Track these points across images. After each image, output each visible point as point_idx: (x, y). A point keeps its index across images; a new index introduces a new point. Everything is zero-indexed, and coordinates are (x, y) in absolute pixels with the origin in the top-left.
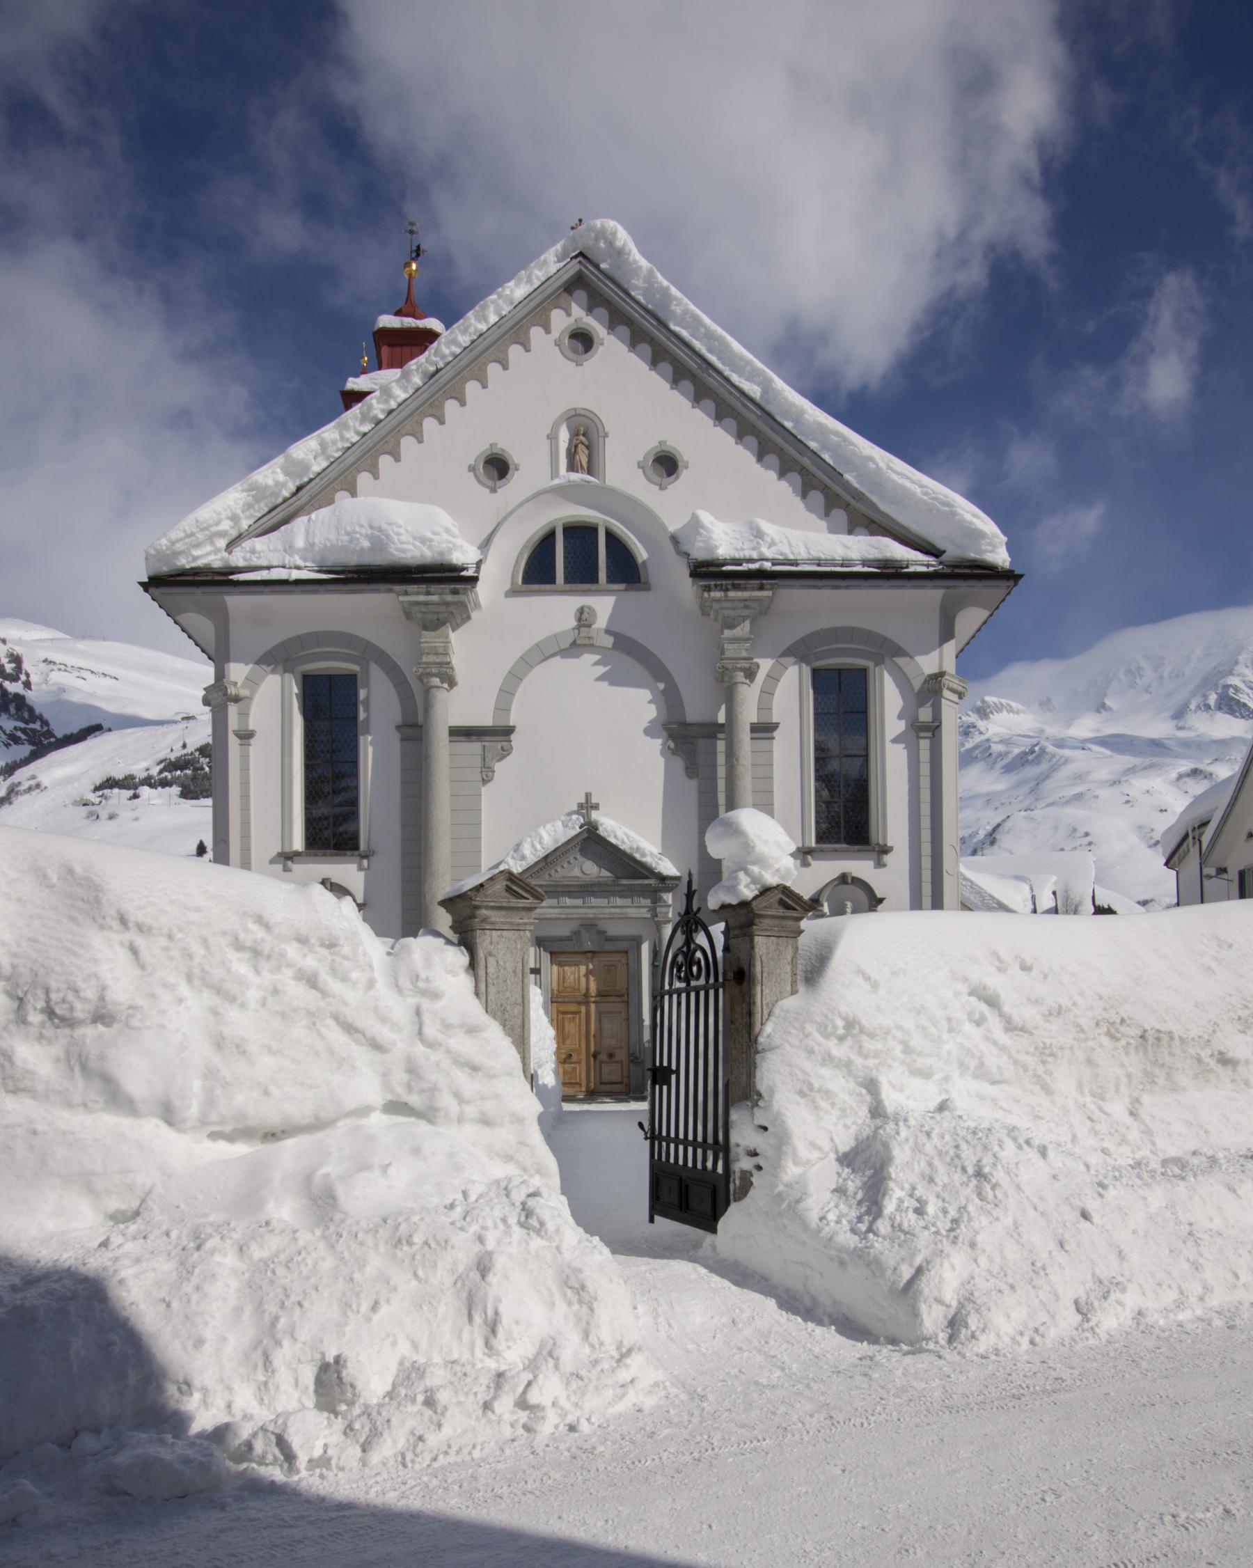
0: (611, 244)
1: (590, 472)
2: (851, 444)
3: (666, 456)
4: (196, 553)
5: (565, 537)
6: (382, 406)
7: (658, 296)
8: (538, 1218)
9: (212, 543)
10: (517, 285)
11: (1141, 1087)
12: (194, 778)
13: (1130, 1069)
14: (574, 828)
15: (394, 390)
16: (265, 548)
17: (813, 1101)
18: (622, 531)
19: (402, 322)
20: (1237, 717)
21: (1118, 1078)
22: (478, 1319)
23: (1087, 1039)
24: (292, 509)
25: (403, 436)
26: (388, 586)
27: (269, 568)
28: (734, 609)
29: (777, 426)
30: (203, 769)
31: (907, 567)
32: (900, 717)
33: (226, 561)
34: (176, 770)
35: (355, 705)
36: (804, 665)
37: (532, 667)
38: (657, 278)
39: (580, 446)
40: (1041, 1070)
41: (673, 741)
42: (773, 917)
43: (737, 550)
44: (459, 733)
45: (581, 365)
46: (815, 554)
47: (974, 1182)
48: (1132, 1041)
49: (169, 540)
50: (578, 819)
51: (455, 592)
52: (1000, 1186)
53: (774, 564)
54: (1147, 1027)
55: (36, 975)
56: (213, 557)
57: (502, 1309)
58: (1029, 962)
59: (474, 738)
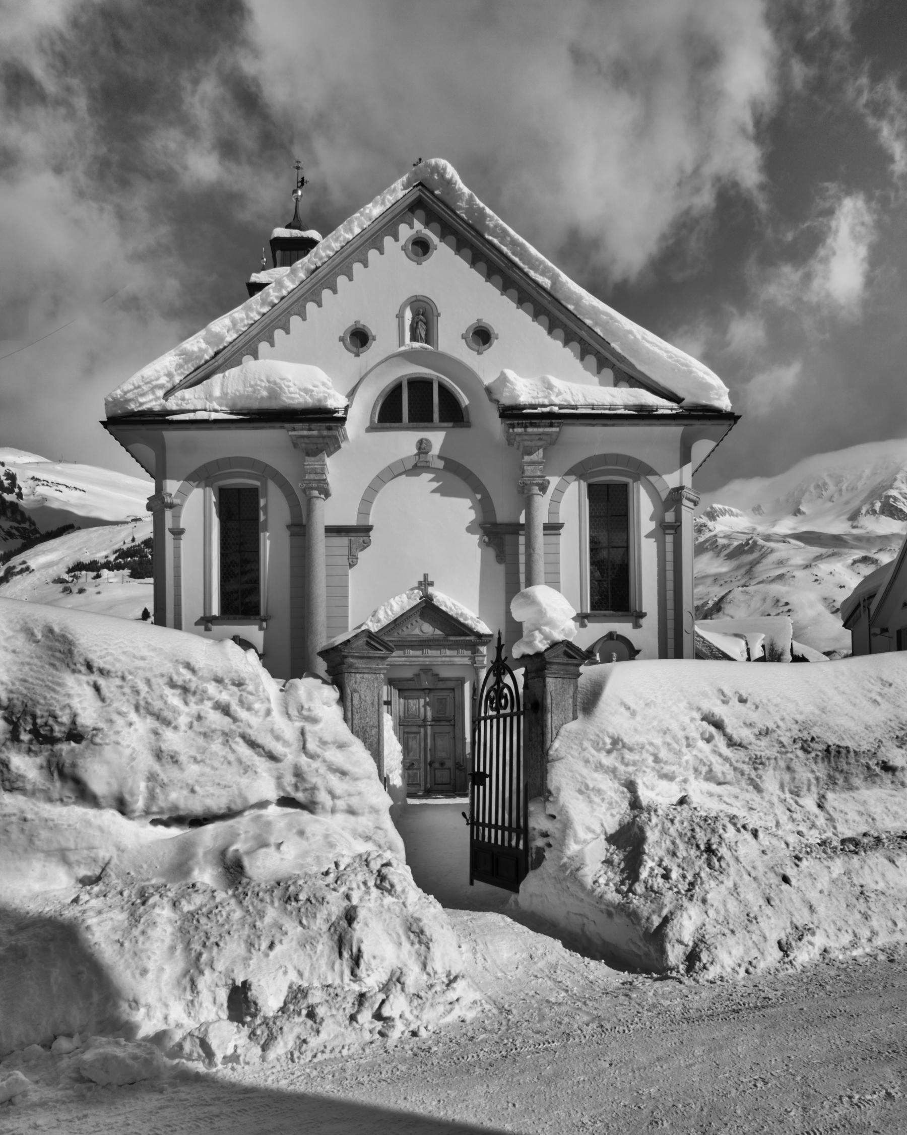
1: (427, 342)
2: (616, 321)
4: (142, 400)
6: (276, 294)
9: (154, 393)
10: (374, 206)
13: (818, 774)
16: (192, 396)
17: (589, 797)
21: (809, 780)
22: (346, 955)
23: (787, 752)
24: (211, 368)
27: (194, 411)
32: (651, 519)
36: (582, 482)
40: (753, 774)
43: (533, 398)
44: (333, 531)
46: (591, 401)
48: (820, 754)
49: (122, 391)
51: (329, 429)
53: (560, 408)
54: (830, 743)
59: (343, 534)
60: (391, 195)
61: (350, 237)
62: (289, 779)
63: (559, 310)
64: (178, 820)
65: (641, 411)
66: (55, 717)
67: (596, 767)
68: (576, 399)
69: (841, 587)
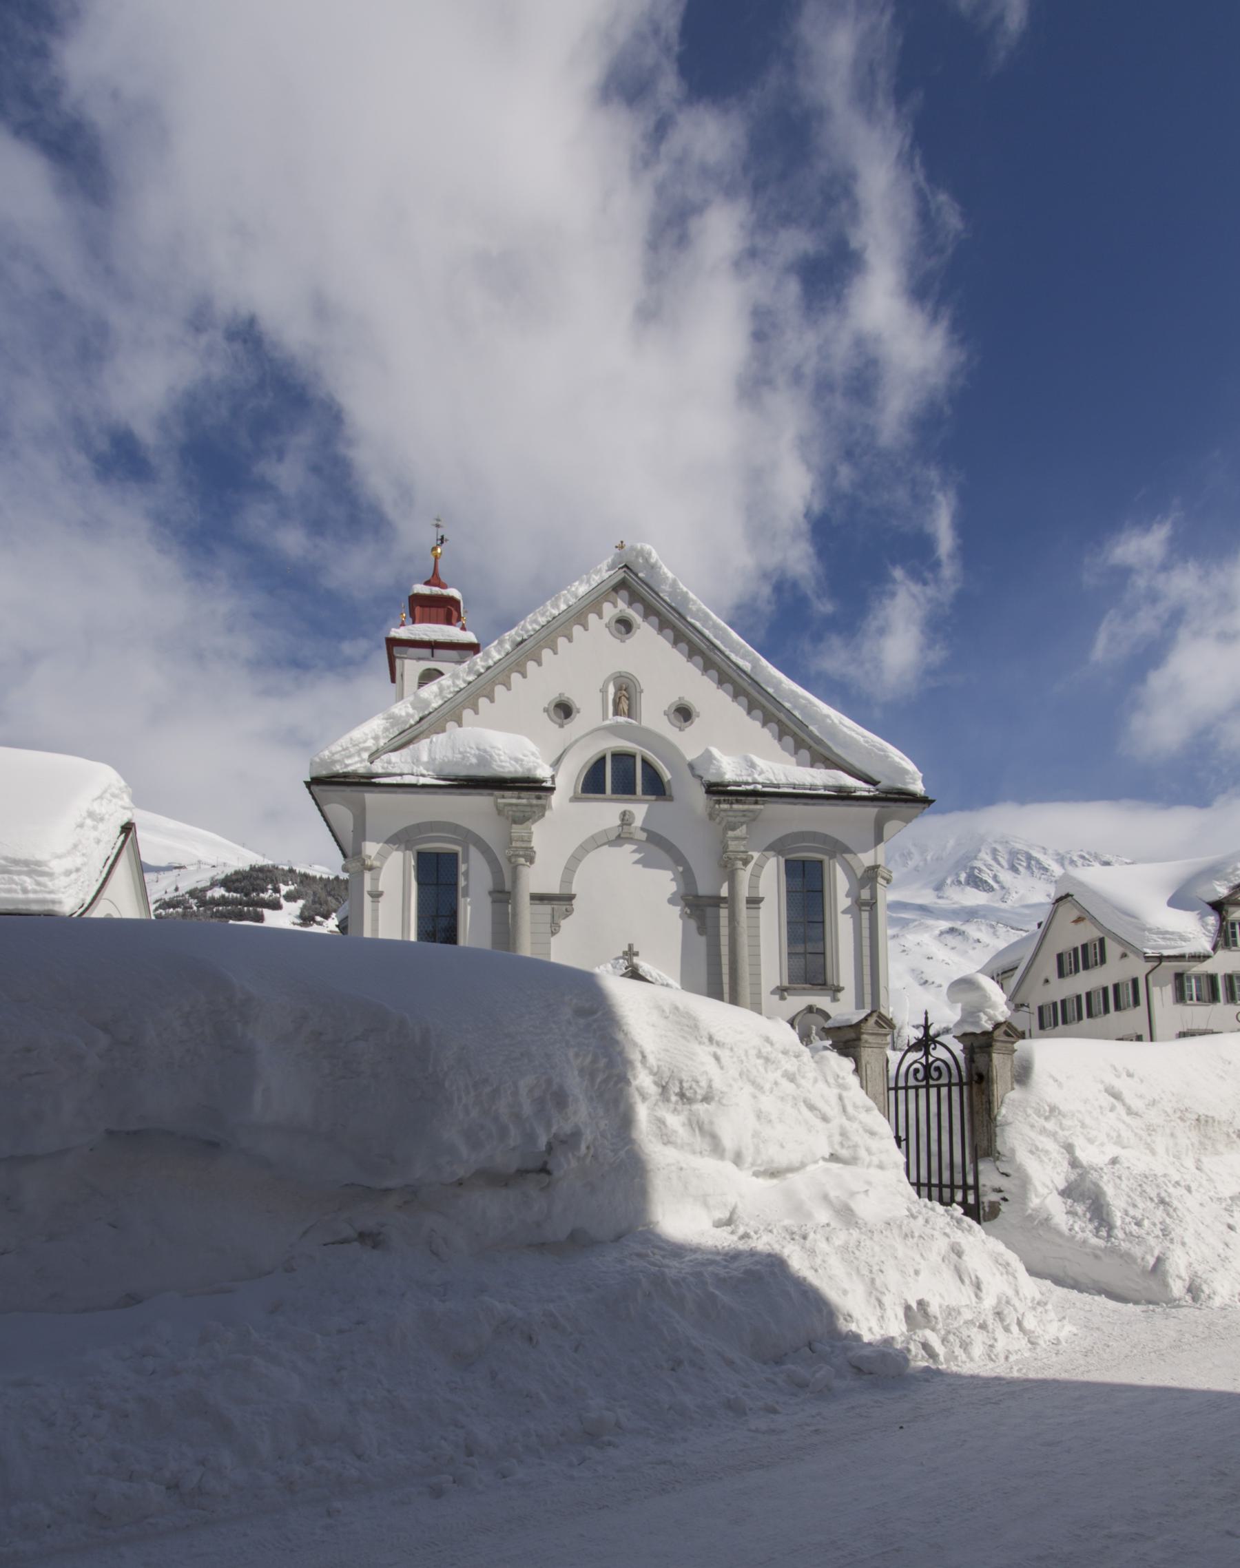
0: (647, 560)
1: (629, 716)
2: (815, 706)
3: (684, 708)
4: (348, 762)
5: (612, 761)
6: (483, 664)
7: (679, 598)
8: (967, 1223)
9: (359, 755)
10: (580, 584)
11: (1198, 1152)
12: (184, 915)
13: (1193, 1140)
14: (621, 969)
15: (492, 653)
16: (398, 760)
17: (1039, 1157)
18: (654, 759)
19: (431, 590)
20: (980, 890)
21: (1187, 1146)
22: (967, 1281)
23: (1171, 1121)
24: (416, 733)
25: (497, 684)
26: (490, 791)
27: (401, 775)
28: (735, 817)
29: (762, 691)
30: (191, 908)
31: (855, 792)
32: (847, 896)
33: (369, 769)
34: (169, 908)
35: (456, 875)
36: (780, 857)
37: (588, 852)
38: (678, 585)
39: (623, 697)
40: (1149, 1140)
41: (689, 908)
42: (1002, 1041)
43: (737, 775)
45: (624, 642)
46: (792, 780)
47: (1162, 1207)
48: (1193, 1122)
49: (330, 752)
50: (624, 963)
51: (539, 798)
52: (1179, 1209)
53: (763, 787)
54: (1200, 1113)
55: (673, 1072)
56: (359, 765)
57: (979, 1276)
58: (1131, 1071)
59: (546, 902)
60: (596, 575)
61: (556, 612)
62: (837, 1138)
63: (759, 693)
64: (774, 1173)
65: (840, 791)
66: (697, 1082)
67: (1041, 1130)
68: (778, 778)
69: (928, 958)
